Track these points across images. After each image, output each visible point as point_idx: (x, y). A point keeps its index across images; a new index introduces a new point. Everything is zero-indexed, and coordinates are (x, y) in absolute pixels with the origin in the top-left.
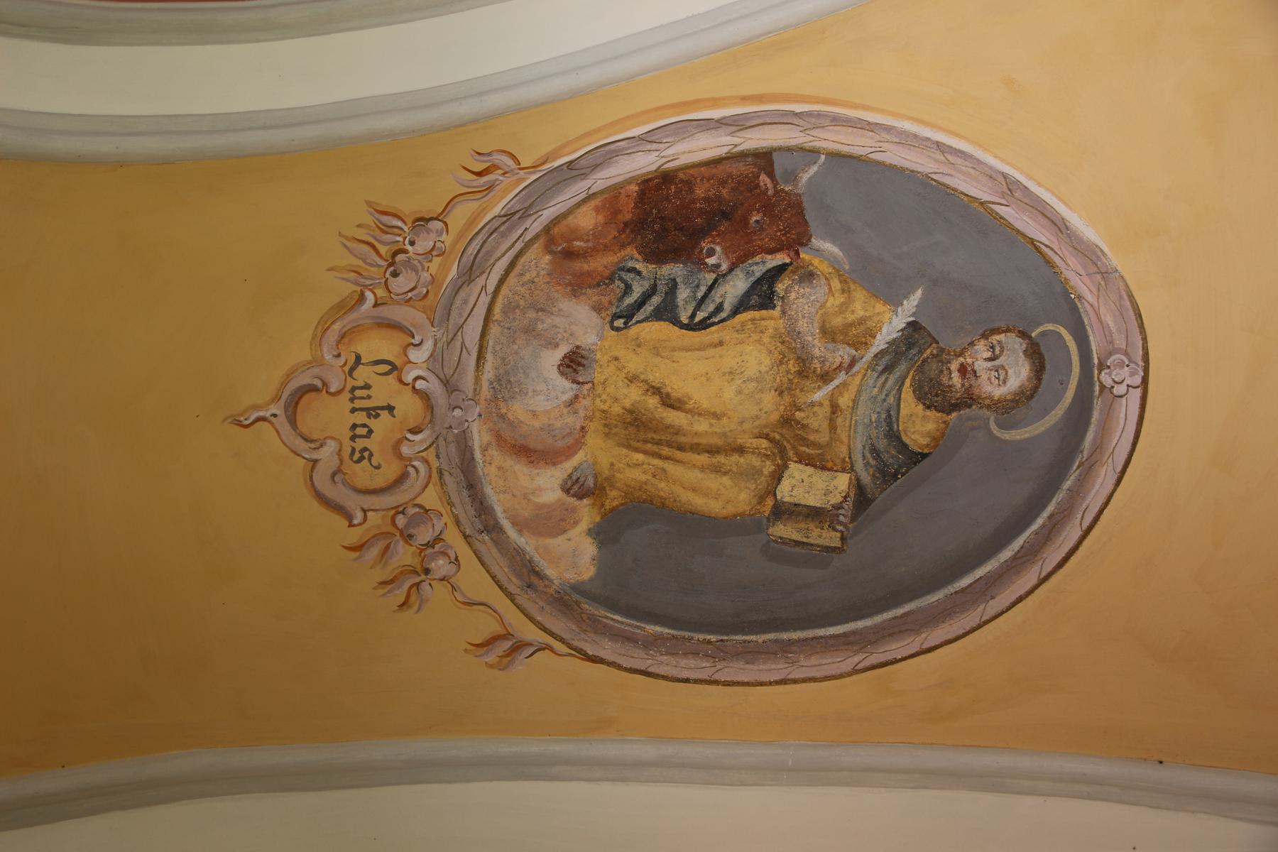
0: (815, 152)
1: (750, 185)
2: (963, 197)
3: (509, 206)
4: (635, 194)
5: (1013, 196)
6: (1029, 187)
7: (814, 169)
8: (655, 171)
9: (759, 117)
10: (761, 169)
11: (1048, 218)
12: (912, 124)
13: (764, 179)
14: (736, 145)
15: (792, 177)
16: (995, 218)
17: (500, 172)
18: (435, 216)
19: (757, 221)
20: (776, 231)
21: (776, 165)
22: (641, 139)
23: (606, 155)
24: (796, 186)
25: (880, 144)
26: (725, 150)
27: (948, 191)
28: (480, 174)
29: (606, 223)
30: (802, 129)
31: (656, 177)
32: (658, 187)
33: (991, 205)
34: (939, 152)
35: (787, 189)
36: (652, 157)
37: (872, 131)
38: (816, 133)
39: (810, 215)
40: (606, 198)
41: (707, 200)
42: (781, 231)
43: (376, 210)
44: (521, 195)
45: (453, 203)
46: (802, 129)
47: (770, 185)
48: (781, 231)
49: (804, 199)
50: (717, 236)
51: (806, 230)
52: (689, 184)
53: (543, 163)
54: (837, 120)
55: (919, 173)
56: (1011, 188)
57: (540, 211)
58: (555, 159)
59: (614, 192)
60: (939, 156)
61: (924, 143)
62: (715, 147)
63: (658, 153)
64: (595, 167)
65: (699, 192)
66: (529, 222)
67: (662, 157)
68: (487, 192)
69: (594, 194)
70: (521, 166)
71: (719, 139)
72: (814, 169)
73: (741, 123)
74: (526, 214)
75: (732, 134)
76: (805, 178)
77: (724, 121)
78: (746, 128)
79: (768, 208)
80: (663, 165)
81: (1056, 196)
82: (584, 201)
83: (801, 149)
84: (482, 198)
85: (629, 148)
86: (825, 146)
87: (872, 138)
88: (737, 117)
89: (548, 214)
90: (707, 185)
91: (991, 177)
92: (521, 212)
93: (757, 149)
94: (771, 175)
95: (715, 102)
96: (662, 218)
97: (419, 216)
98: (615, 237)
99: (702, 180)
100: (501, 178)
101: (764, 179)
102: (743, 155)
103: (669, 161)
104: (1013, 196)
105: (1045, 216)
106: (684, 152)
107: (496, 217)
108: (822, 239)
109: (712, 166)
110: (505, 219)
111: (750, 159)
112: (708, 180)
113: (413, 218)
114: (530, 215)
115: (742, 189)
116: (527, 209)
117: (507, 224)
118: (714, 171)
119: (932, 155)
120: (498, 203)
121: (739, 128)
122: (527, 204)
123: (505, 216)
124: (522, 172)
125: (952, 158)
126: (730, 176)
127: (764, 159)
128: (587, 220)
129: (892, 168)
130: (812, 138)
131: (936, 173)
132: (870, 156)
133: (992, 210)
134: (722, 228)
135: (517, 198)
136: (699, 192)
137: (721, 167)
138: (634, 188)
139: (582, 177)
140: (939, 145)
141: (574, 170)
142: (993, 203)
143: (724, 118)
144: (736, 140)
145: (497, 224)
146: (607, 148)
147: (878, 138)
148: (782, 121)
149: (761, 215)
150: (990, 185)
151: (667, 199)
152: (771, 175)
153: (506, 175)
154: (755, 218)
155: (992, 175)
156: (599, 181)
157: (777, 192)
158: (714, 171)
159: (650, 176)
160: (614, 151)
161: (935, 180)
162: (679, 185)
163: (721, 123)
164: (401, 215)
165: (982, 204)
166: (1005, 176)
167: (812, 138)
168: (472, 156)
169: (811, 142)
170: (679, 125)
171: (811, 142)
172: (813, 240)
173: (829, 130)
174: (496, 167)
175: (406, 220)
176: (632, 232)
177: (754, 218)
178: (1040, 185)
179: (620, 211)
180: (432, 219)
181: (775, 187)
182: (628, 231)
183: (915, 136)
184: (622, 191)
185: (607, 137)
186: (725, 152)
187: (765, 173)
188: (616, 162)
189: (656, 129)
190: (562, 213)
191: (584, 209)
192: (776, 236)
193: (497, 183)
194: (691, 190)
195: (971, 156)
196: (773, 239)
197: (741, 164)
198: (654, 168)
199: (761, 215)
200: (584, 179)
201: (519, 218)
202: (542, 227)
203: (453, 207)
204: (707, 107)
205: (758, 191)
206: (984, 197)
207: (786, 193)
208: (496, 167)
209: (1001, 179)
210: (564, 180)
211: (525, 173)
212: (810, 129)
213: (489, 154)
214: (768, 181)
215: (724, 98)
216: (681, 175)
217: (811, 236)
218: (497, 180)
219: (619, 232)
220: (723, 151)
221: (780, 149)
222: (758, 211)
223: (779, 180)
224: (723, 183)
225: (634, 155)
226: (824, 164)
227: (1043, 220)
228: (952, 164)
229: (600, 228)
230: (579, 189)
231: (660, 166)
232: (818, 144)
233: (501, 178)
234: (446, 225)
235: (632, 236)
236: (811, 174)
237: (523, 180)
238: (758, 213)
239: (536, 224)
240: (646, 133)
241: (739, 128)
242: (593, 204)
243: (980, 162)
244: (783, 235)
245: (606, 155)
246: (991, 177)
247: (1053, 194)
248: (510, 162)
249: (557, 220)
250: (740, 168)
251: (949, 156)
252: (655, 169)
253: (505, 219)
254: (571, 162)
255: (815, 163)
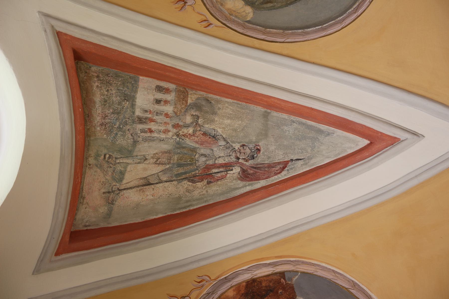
0: (297, 272)
1: (279, 282)
2: (340, 286)
3: (208, 291)
4: (245, 286)
5: (355, 287)
6: (360, 285)
7: (297, 277)
8: (251, 279)
9: (281, 262)
10: (281, 277)
11: (365, 294)
12: (325, 264)
13: (282, 280)
14: (274, 271)
15: (291, 279)
16: (350, 293)
17: (205, 281)
18: (187, 296)
19: (281, 292)
20: (286, 295)
21: (286, 276)
22: (246, 270)
23: (236, 275)
24: (292, 282)
25: (316, 270)
26: (271, 272)
27: (336, 284)
28: (199, 282)
29: (237, 294)
30: (293, 265)
31: (251, 281)
32: (252, 283)
33: (349, 289)
34: (333, 273)
35: (289, 283)
36: (250, 275)
37: (313, 266)
38: (298, 266)
39: (296, 290)
40: (236, 287)
41: (266, 287)
42: (288, 295)
43: (169, 296)
44: (211, 288)
45: (192, 291)
46: (293, 265)
47: (284, 282)
48: (288, 295)
49: (294, 286)
50: (269, 297)
51: (295, 294)
52: (261, 282)
53: (217, 278)
54: (303, 263)
55: (328, 278)
56: (355, 285)
57: (217, 292)
58: (221, 277)
59: (239, 285)
60: (333, 274)
61: (329, 270)
62: (268, 271)
63: (251, 274)
64: (233, 278)
65: (264, 284)
66: (214, 295)
67: (253, 275)
68: (201, 287)
69: (233, 286)
70: (211, 279)
71: (269, 269)
72: (297, 277)
73: (275, 264)
74: (213, 293)
75: (273, 267)
76: (294, 279)
77: (270, 264)
78: (277, 266)
79: (284, 288)
80: (253, 277)
81: (368, 288)
82: (230, 288)
83: (293, 271)
84: (201, 289)
85: (243, 272)
86: (300, 270)
87: (314, 268)
88: (274, 263)
89: (219, 293)
90: (266, 282)
91: (349, 281)
92: (212, 292)
93: (280, 271)
94: (284, 279)
95: (268, 259)
96: (253, 292)
97: (182, 296)
98: (239, 298)
99: (264, 281)
100: (206, 283)
101: (282, 280)
102: (276, 274)
103: (254, 276)
104: (355, 287)
105: (365, 294)
106: (259, 273)
107: (204, 294)
108: (300, 297)
109: (267, 277)
110: (207, 295)
111: (278, 274)
112: (266, 281)
113: (181, 296)
114: (215, 293)
115: (276, 283)
116: (213, 291)
117: (208, 296)
118: (268, 278)
119: (331, 274)
120: (205, 290)
121: (275, 265)
122: (213, 290)
123: (207, 294)
124: (211, 281)
125: (337, 275)
126: (273, 279)
127: (282, 274)
128: (231, 293)
129: (320, 276)
130: (296, 268)
131: (333, 279)
132: (313, 273)
133: (349, 290)
134: (271, 294)
135: (210, 289)
136: (264, 284)
137: (270, 277)
138: (244, 284)
139: (229, 281)
140: (333, 271)
141: (227, 280)
142: (349, 289)
143: (271, 263)
144: (274, 269)
145: (205, 296)
146: (236, 273)
147: (315, 268)
148: (287, 263)
149: (282, 290)
150: (348, 283)
151: (254, 286)
152: (284, 279)
153: (207, 282)
154: (280, 291)
155: (349, 281)
156: (234, 282)
157: (286, 284)
158: (268, 278)
159: (249, 280)
160: (238, 273)
161: (332, 281)
162: (258, 283)
163: (269, 264)
164: (177, 296)
165: (346, 288)
166: (353, 281)
167: (296, 268)
168: (197, 277)
169: (296, 269)
170: (257, 265)
171: (296, 269)
172: (297, 297)
173: (301, 266)
174: (204, 280)
175: (178, 297)
176: (244, 296)
177: (280, 291)
178: (363, 285)
179: (241, 291)
180: (186, 296)
181: (286, 282)
182: (243, 296)
183: (326, 268)
184: (241, 285)
185: (236, 269)
186: (271, 273)
187: (283, 278)
188: (239, 276)
189: (250, 267)
190: (224, 292)
191: (230, 290)
192: (286, 296)
193: (205, 284)
194: (261, 284)
195: (343, 275)
196: (285, 297)
197: (276, 276)
198: (250, 278)
199: (282, 290)
200: (229, 282)
201: (211, 294)
202: (218, 296)
203: (192, 293)
204: (265, 260)
205: (281, 284)
206: (347, 287)
207: (289, 284)
208: (204, 280)
209: (351, 282)
210: (224, 282)
211: (212, 281)
212: (296, 265)
213: (202, 276)
214: (284, 280)
215: (270, 257)
216: (258, 280)
217: (296, 296)
218: (204, 284)
219: (240, 296)
220: (270, 273)
221: (287, 271)
222: (281, 289)
223: (287, 280)
224: (270, 282)
225: (244, 275)
226: (300, 275)
227: (364, 295)
228: (337, 277)
229: (235, 296)
230: (228, 285)
231: (252, 277)
232: (298, 270)
233: (206, 283)
234: (190, 297)
235: (244, 297)
236: (296, 278)
237: (212, 283)
238: (281, 290)
239: (216, 295)
240: (248, 268)
241: (275, 265)
242: (232, 289)
243: (345, 276)
244: (288, 296)
245: (236, 275)
246: (349, 281)
247: (367, 288)
248: (208, 278)
249: (222, 294)
250: (275, 277)
251: (336, 274)
252: (250, 278)
253: (207, 295)
254: (226, 277)
255: (297, 275)
